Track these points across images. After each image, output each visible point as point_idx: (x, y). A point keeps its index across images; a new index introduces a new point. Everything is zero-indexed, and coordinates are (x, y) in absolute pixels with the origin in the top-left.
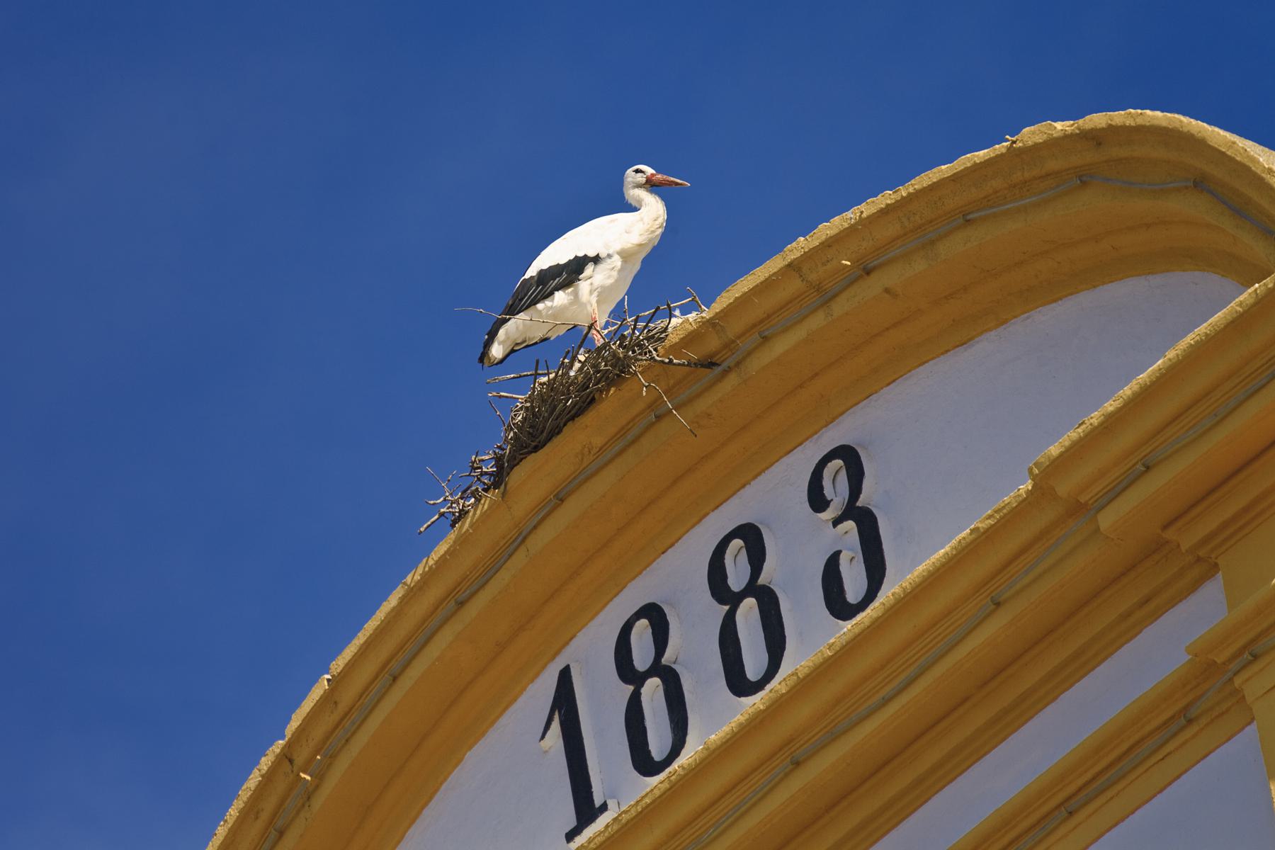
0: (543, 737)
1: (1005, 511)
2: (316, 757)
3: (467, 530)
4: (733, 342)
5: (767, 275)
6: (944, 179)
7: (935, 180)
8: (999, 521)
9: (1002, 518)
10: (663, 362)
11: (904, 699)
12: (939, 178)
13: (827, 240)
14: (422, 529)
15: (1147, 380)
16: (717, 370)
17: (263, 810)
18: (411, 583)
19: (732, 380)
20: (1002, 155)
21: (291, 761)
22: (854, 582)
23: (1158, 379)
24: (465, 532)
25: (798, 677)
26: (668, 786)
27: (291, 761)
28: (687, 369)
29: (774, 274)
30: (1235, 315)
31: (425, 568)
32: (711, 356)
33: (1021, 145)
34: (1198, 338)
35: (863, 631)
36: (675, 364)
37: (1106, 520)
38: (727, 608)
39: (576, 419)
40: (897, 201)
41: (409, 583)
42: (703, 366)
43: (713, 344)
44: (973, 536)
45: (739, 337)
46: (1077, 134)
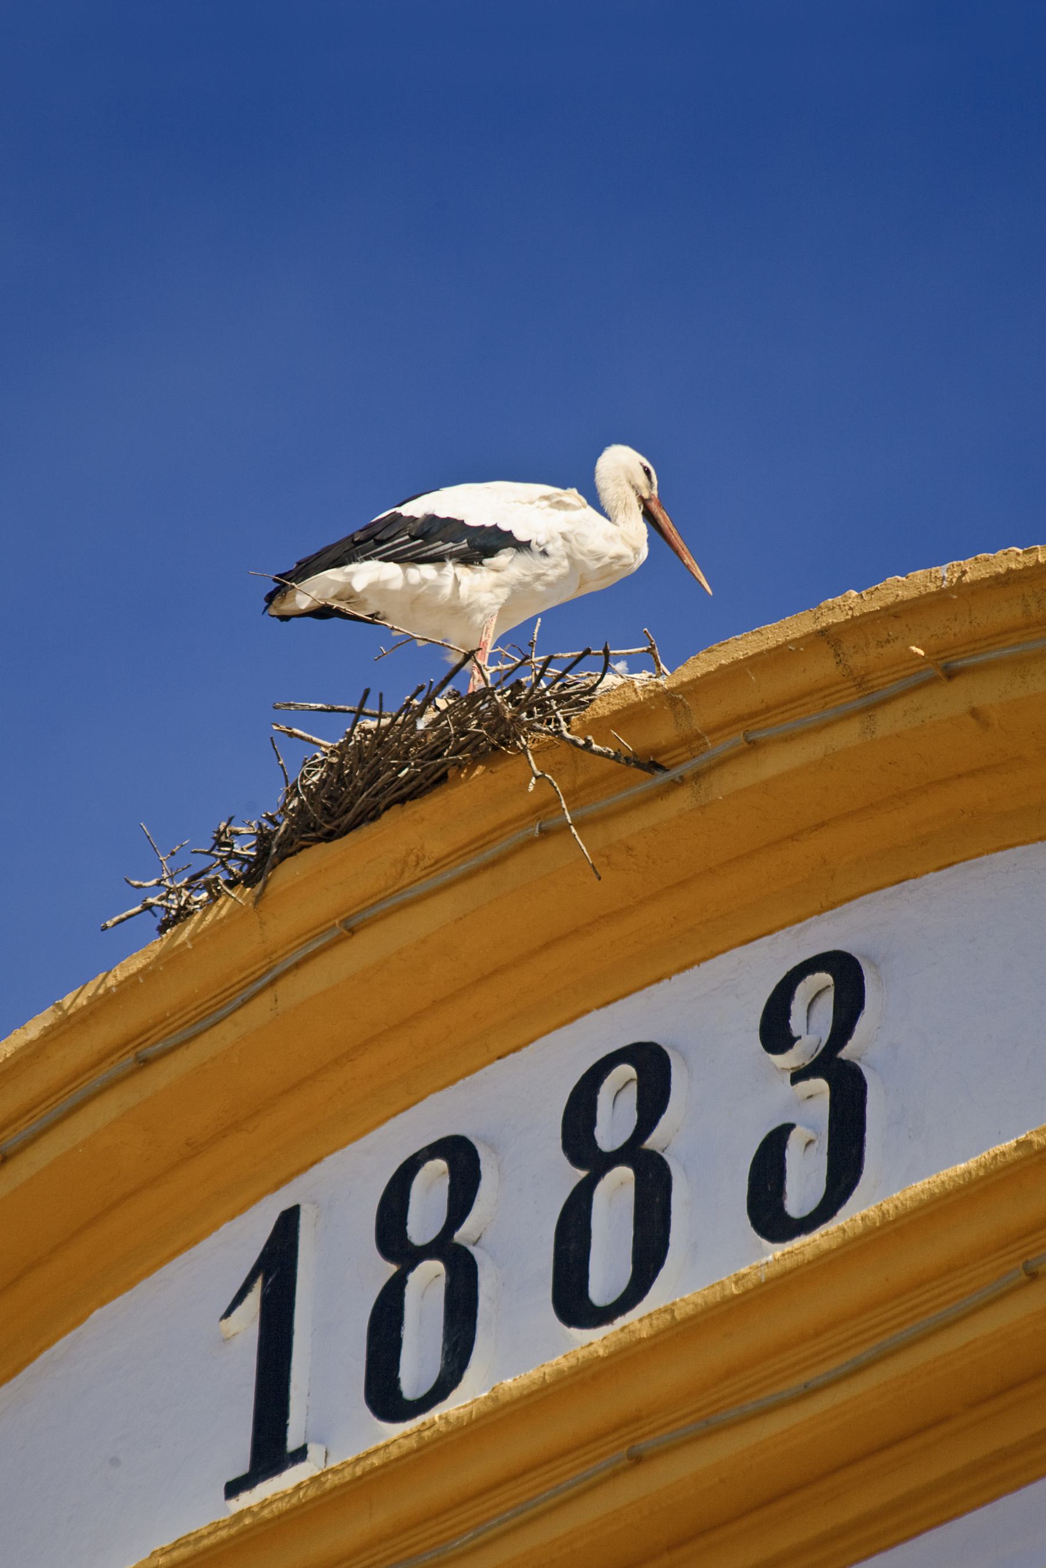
0: (228, 1314)
3: (184, 944)
4: (699, 737)
13: (895, 605)
18: (70, 1007)
31: (98, 988)
35: (799, 1267)
36: (593, 751)
39: (408, 803)
40: (1026, 568)
42: (639, 765)
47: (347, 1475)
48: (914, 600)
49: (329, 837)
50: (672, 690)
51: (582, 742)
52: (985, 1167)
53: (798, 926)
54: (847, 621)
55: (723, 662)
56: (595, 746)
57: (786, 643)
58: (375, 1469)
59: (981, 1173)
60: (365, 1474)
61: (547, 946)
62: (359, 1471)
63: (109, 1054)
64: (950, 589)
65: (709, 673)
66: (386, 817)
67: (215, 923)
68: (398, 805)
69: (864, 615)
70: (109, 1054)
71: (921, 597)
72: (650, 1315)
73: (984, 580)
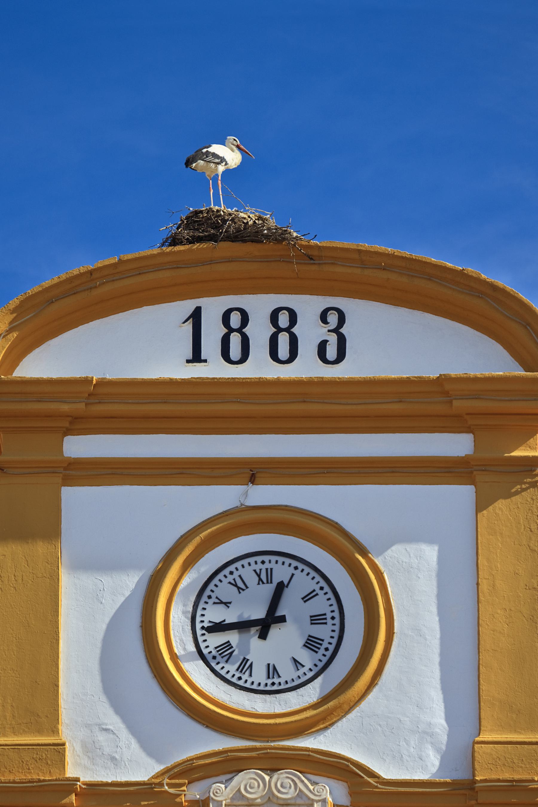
0: (184, 323)
1: (422, 379)
2: (520, 491)
3: (194, 249)
4: (322, 256)
5: (349, 247)
6: (431, 263)
7: (428, 261)
8: (419, 381)
9: (420, 381)
10: (298, 248)
11: (354, 407)
12: (429, 262)
13: (377, 252)
14: (161, 229)
15: (496, 376)
16: (312, 262)
17: (74, 282)
18: (165, 250)
19: (314, 268)
20: (457, 271)
21: (91, 274)
22: (331, 353)
23: (499, 378)
24: (193, 249)
25: (323, 380)
26: (258, 381)
27: (91, 274)
28: (303, 254)
29: (351, 249)
30: (535, 377)
31: (172, 249)
32: (312, 256)
33: (466, 272)
34: (519, 375)
35: (353, 381)
36: (301, 252)
37: (456, 403)
38: (275, 330)
39: (254, 243)
40: (410, 258)
41: (164, 250)
42: (309, 257)
43: (315, 253)
44: (407, 379)
45: (324, 257)
46: (490, 284)
47: (241, 380)
48: (382, 253)
49: (233, 241)
50: (320, 246)
51: (300, 249)
52: (399, 379)
53: (324, 297)
54: (365, 250)
55: (334, 246)
56: (302, 251)
57: (350, 248)
58: (247, 382)
59: (398, 380)
60: (245, 382)
61: (267, 278)
62: (244, 381)
63: (170, 262)
64: (391, 254)
65: (330, 247)
66: (248, 243)
67: (202, 248)
68: (251, 242)
69: (369, 251)
70: (170, 262)
71: (384, 253)
72: (317, 377)
73: (399, 256)
